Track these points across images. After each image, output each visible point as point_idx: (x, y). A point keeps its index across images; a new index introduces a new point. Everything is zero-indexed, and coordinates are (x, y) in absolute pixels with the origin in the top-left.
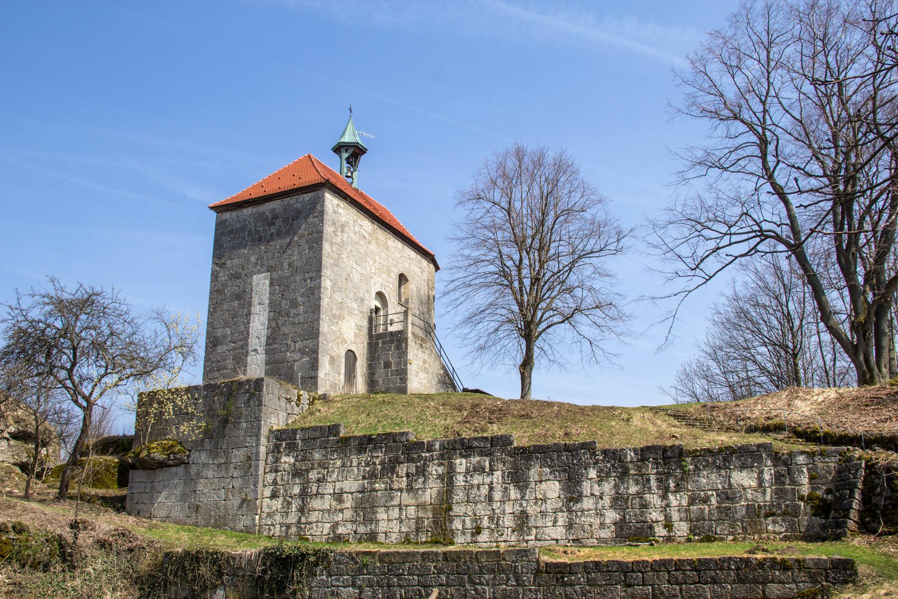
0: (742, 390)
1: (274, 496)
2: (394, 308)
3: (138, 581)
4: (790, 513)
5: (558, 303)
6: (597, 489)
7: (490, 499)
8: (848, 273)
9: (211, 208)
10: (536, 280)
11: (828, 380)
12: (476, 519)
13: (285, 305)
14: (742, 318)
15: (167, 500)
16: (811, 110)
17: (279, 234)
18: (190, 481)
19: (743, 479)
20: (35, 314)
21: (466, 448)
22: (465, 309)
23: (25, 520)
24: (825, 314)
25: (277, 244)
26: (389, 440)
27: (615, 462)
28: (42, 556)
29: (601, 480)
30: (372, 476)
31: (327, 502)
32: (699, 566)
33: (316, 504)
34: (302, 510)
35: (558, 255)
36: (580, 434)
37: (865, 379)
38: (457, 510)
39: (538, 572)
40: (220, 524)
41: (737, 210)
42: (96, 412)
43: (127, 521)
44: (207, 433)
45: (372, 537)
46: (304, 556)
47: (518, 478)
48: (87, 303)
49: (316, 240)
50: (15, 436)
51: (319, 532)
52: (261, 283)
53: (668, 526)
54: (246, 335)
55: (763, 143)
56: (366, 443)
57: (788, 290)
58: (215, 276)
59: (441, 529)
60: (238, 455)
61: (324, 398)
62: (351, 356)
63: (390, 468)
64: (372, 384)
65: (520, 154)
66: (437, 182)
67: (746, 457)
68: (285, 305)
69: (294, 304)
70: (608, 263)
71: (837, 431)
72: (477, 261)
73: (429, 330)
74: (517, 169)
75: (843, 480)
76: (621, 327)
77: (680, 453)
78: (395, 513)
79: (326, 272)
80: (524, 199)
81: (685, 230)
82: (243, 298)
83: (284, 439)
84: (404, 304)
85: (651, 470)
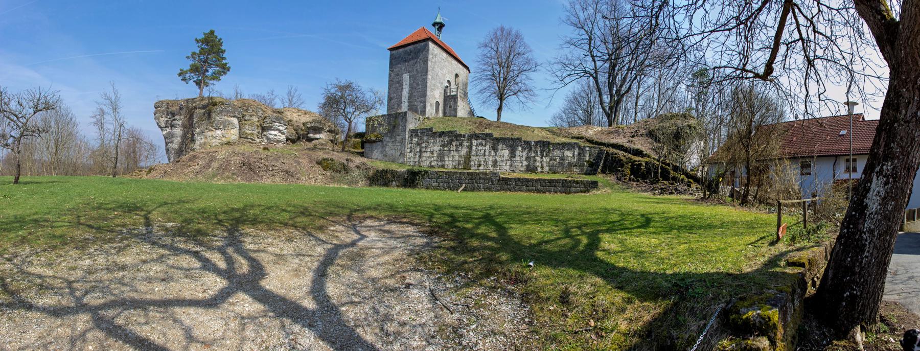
0: (572, 124)
2: (453, 86)
3: (369, 178)
4: (582, 166)
5: (512, 88)
6: (521, 153)
7: (484, 155)
8: (611, 90)
10: (505, 79)
11: (600, 124)
12: (479, 161)
13: (415, 85)
14: (575, 100)
15: (376, 153)
16: (607, 31)
17: (412, 59)
18: (384, 147)
19: (568, 153)
20: (332, 91)
21: (477, 137)
22: (479, 88)
23: (333, 157)
24: (602, 103)
25: (412, 62)
26: (450, 133)
27: (528, 145)
28: (339, 168)
29: (523, 151)
30: (444, 145)
31: (428, 154)
32: (551, 181)
33: (424, 155)
34: (420, 157)
35: (514, 70)
36: (517, 135)
37: (610, 125)
38: (473, 158)
39: (499, 180)
40: (393, 161)
41: (579, 62)
42: (353, 124)
43: (365, 160)
44: (389, 131)
45: (443, 166)
46: (420, 172)
47: (494, 148)
48: (348, 87)
49: (426, 61)
50: (329, 131)
51: (425, 164)
52: (406, 77)
53: (542, 168)
54: (401, 96)
55: (590, 39)
56: (442, 134)
57: (591, 93)
58: (390, 75)
59: (467, 165)
60: (399, 138)
61: (428, 118)
62: (437, 103)
63: (450, 143)
64: (445, 113)
65: (502, 29)
66: (470, 41)
67: (570, 146)
68: (415, 85)
69: (418, 85)
70: (531, 75)
71: (600, 141)
72: (484, 70)
73: (466, 94)
74: (502, 35)
75: (599, 157)
76: (533, 98)
77: (549, 143)
78: (451, 158)
79: (429, 73)
80: (503, 47)
81: (560, 66)
82: (400, 83)
83: (414, 132)
84: (457, 85)
85: (538, 149)
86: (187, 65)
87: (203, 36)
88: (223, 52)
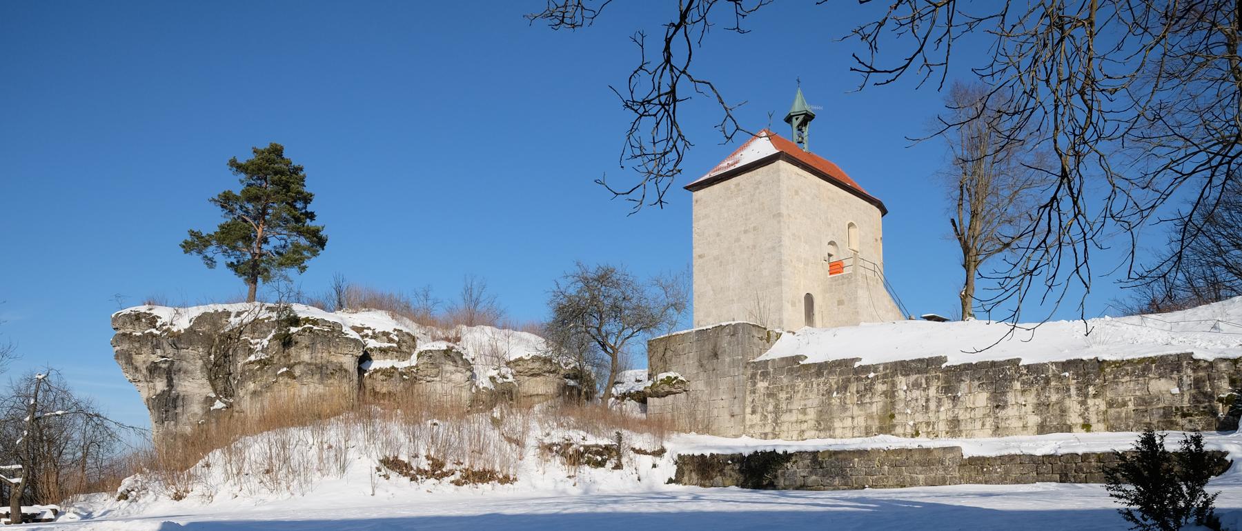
1: (753, 412)
20: (572, 291)
33: (785, 417)
34: (775, 421)
48: (604, 278)
56: (821, 369)
63: (843, 388)
78: (848, 422)
86: (212, 220)
87: (252, 157)
88: (307, 199)
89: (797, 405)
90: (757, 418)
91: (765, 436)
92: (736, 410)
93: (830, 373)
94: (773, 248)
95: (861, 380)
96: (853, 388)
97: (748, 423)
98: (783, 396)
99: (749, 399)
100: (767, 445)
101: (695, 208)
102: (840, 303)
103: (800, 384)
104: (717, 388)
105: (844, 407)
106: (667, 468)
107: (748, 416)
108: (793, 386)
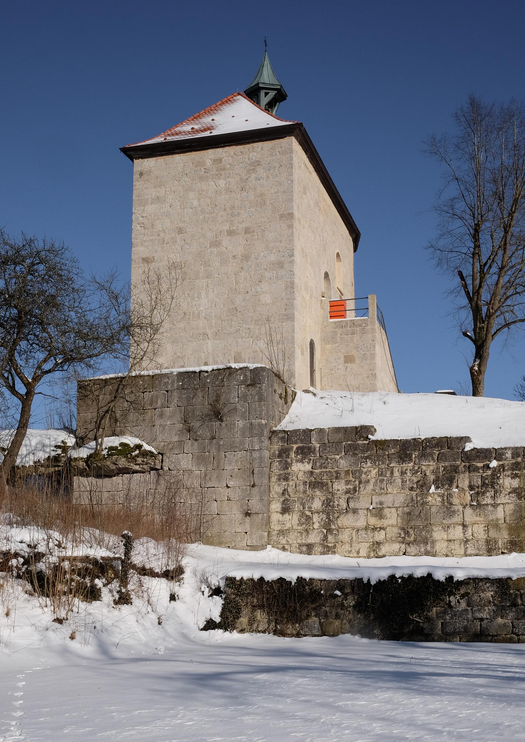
1: (285, 510)
9: (369, 580)
33: (346, 521)
63: (447, 479)
89: (363, 502)
90: (292, 520)
91: (309, 549)
92: (255, 504)
93: (423, 456)
94: (280, 265)
95: (476, 469)
96: (464, 480)
97: (275, 527)
98: (340, 486)
99: (277, 488)
100: (413, 564)
101: (138, 185)
102: (349, 359)
103: (370, 470)
104: (219, 468)
105: (448, 507)
106: (199, 606)
107: (276, 517)
108: (357, 474)
